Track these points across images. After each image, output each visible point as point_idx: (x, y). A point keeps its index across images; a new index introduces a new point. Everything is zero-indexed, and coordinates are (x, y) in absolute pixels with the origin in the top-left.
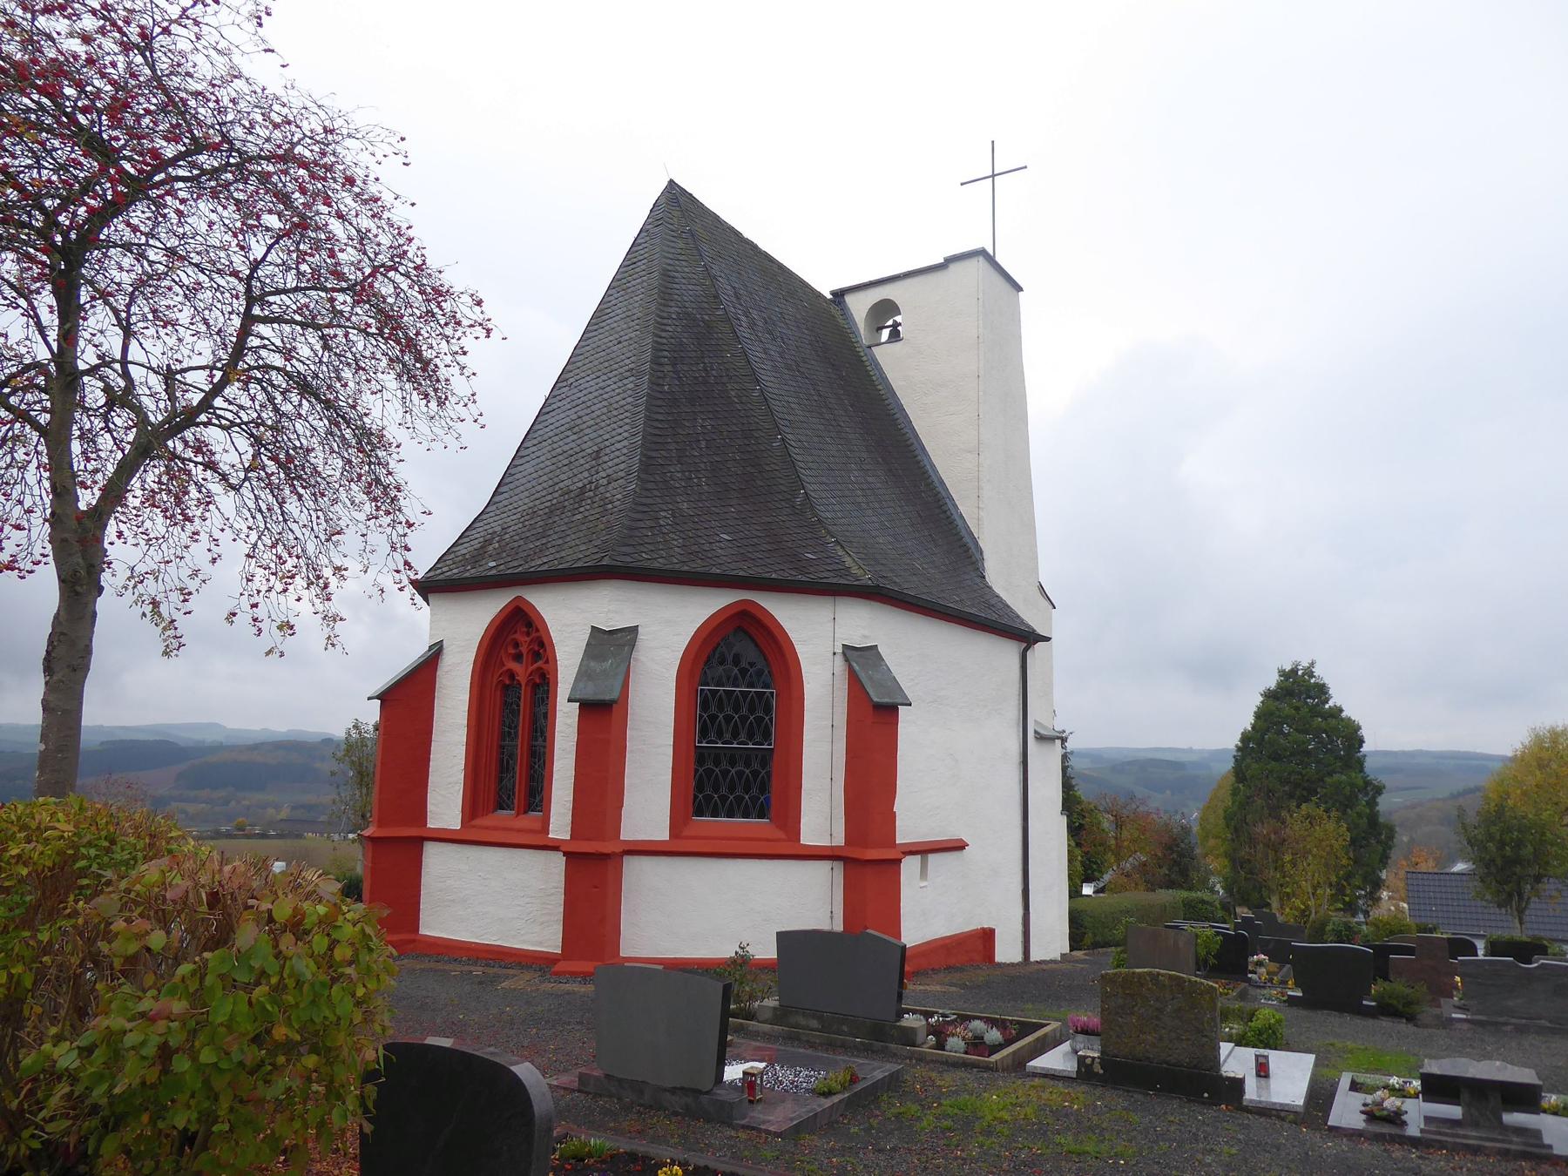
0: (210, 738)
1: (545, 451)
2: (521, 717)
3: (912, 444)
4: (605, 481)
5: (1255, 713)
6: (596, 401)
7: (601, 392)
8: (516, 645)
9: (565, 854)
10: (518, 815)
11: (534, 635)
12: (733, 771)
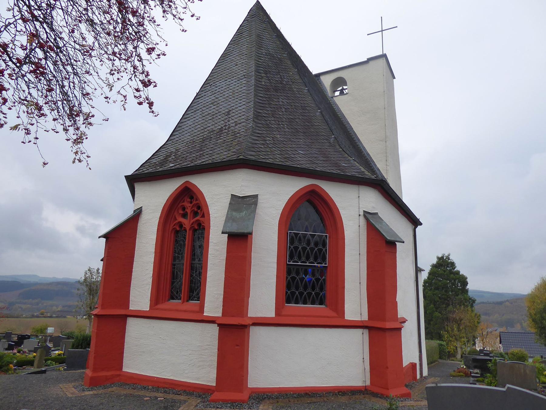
0: (32, 280)
1: (198, 114)
2: (186, 248)
4: (234, 125)
5: (429, 273)
6: (226, 90)
7: (228, 86)
8: (184, 208)
9: (219, 325)
10: (183, 302)
11: (194, 202)
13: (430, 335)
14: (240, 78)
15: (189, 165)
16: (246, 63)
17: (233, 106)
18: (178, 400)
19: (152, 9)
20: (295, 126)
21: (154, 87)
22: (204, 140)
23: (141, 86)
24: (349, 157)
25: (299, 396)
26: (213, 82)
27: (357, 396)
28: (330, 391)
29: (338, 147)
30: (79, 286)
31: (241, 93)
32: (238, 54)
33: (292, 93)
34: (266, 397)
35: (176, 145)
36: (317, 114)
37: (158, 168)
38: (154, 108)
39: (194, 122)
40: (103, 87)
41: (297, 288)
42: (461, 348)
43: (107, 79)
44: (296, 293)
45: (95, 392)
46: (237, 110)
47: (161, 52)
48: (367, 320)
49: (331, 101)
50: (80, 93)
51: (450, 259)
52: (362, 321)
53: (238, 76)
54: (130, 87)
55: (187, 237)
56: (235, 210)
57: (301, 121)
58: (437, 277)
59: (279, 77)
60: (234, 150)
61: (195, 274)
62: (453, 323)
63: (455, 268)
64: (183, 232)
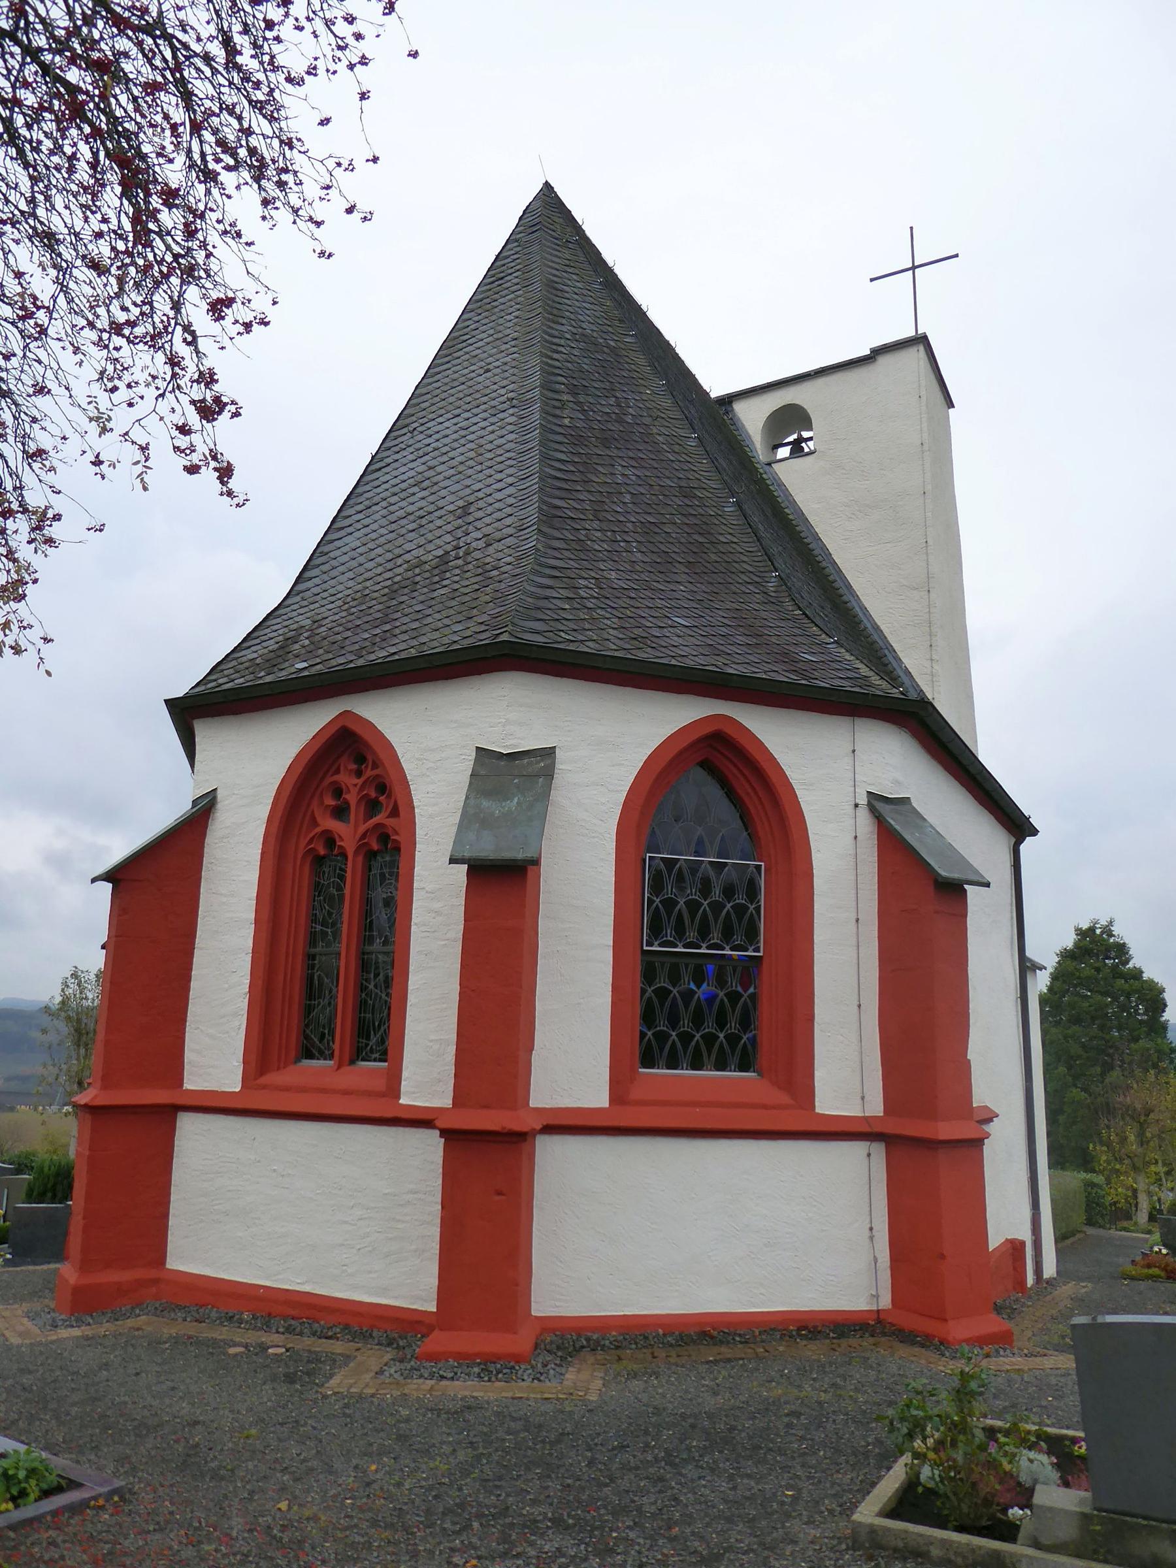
3: (835, 581)
4: (481, 544)
6: (456, 445)
7: (463, 433)
8: (338, 792)
9: (444, 1133)
10: (339, 1068)
11: (369, 773)
13: (1057, 1160)
14: (498, 407)
15: (352, 665)
16: (514, 364)
17: (480, 490)
18: (326, 1352)
19: (229, 197)
20: (661, 546)
21: (232, 417)
22: (393, 592)
23: (193, 419)
24: (824, 636)
25: (682, 1339)
26: (421, 421)
27: (853, 1341)
28: (773, 1326)
29: (789, 605)
30: (46, 1020)
31: (502, 452)
32: (491, 339)
33: (650, 449)
34: (585, 1343)
35: (312, 607)
36: (726, 509)
37: (262, 674)
38: (233, 484)
39: (364, 540)
40: (86, 432)
41: (674, 1021)
42: (1150, 1194)
43: (90, 399)
44: (694, 1036)
45: (87, 1331)
46: (490, 500)
47: (254, 314)
48: (882, 1114)
49: (764, 476)
50: (16, 449)
51: (1114, 936)
52: (866, 1119)
53: (493, 403)
54: (161, 419)
55: (349, 875)
56: (488, 794)
57: (679, 531)
58: (1075, 986)
59: (612, 403)
60: (485, 618)
61: (373, 983)
62: (1123, 1119)
63: (1127, 962)
64: (338, 861)
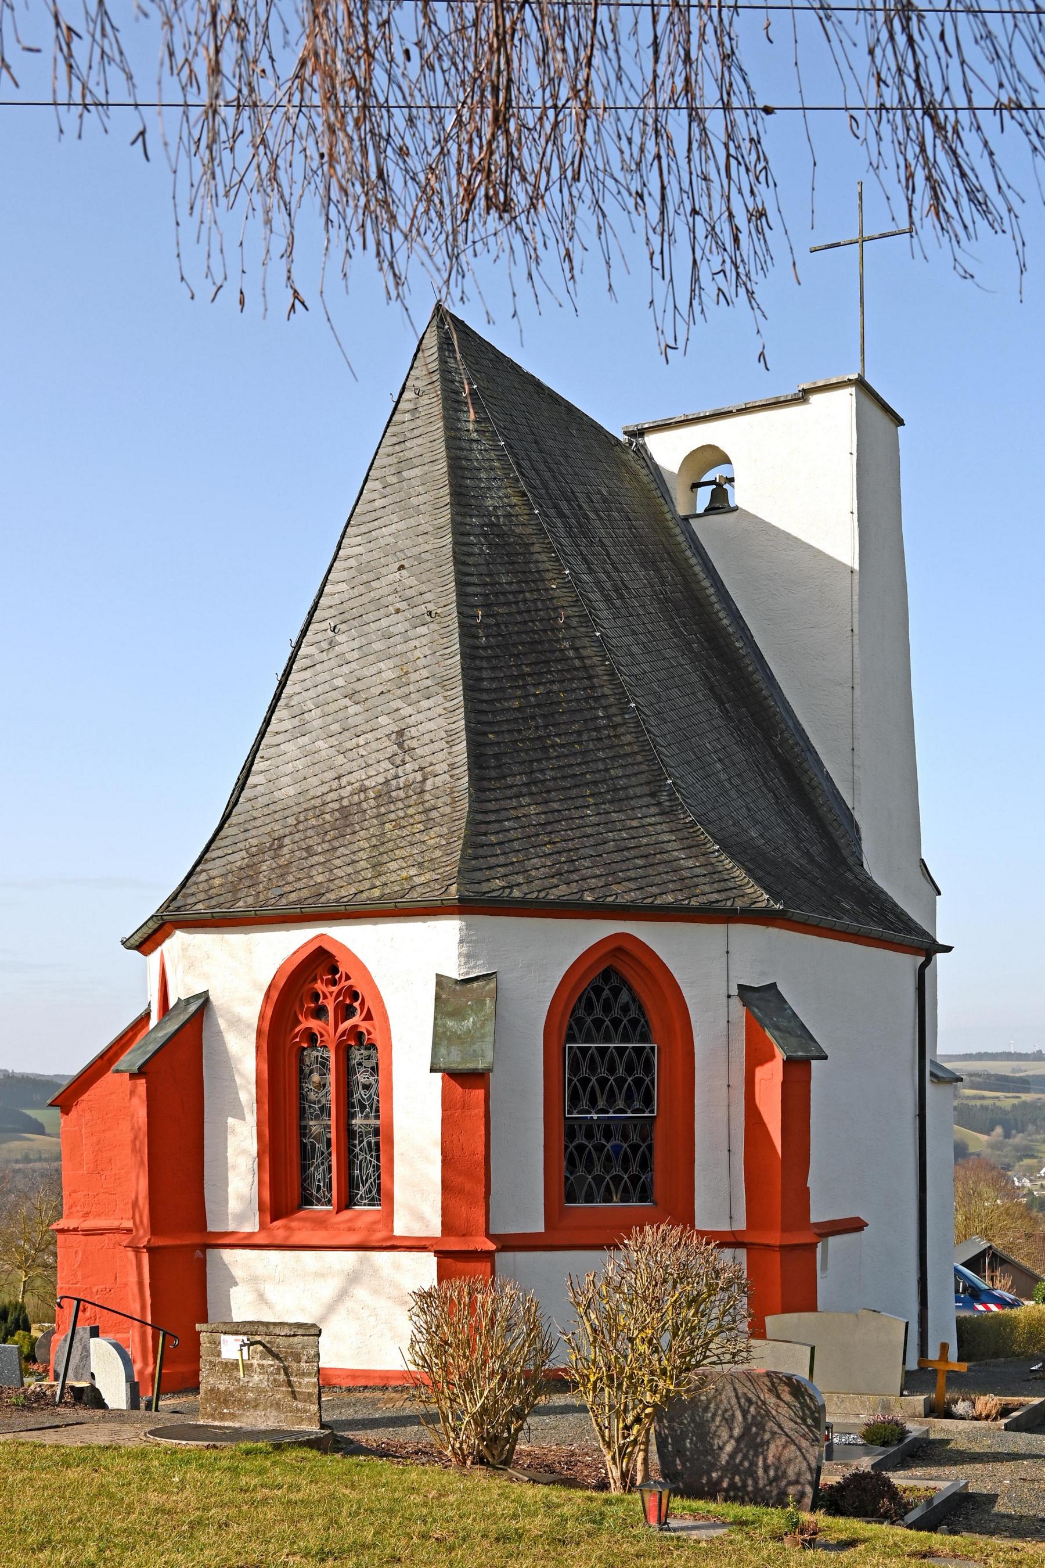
9: (437, 1253)
12: (609, 1146)
